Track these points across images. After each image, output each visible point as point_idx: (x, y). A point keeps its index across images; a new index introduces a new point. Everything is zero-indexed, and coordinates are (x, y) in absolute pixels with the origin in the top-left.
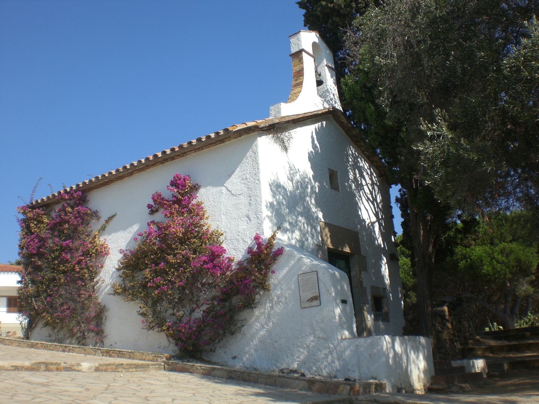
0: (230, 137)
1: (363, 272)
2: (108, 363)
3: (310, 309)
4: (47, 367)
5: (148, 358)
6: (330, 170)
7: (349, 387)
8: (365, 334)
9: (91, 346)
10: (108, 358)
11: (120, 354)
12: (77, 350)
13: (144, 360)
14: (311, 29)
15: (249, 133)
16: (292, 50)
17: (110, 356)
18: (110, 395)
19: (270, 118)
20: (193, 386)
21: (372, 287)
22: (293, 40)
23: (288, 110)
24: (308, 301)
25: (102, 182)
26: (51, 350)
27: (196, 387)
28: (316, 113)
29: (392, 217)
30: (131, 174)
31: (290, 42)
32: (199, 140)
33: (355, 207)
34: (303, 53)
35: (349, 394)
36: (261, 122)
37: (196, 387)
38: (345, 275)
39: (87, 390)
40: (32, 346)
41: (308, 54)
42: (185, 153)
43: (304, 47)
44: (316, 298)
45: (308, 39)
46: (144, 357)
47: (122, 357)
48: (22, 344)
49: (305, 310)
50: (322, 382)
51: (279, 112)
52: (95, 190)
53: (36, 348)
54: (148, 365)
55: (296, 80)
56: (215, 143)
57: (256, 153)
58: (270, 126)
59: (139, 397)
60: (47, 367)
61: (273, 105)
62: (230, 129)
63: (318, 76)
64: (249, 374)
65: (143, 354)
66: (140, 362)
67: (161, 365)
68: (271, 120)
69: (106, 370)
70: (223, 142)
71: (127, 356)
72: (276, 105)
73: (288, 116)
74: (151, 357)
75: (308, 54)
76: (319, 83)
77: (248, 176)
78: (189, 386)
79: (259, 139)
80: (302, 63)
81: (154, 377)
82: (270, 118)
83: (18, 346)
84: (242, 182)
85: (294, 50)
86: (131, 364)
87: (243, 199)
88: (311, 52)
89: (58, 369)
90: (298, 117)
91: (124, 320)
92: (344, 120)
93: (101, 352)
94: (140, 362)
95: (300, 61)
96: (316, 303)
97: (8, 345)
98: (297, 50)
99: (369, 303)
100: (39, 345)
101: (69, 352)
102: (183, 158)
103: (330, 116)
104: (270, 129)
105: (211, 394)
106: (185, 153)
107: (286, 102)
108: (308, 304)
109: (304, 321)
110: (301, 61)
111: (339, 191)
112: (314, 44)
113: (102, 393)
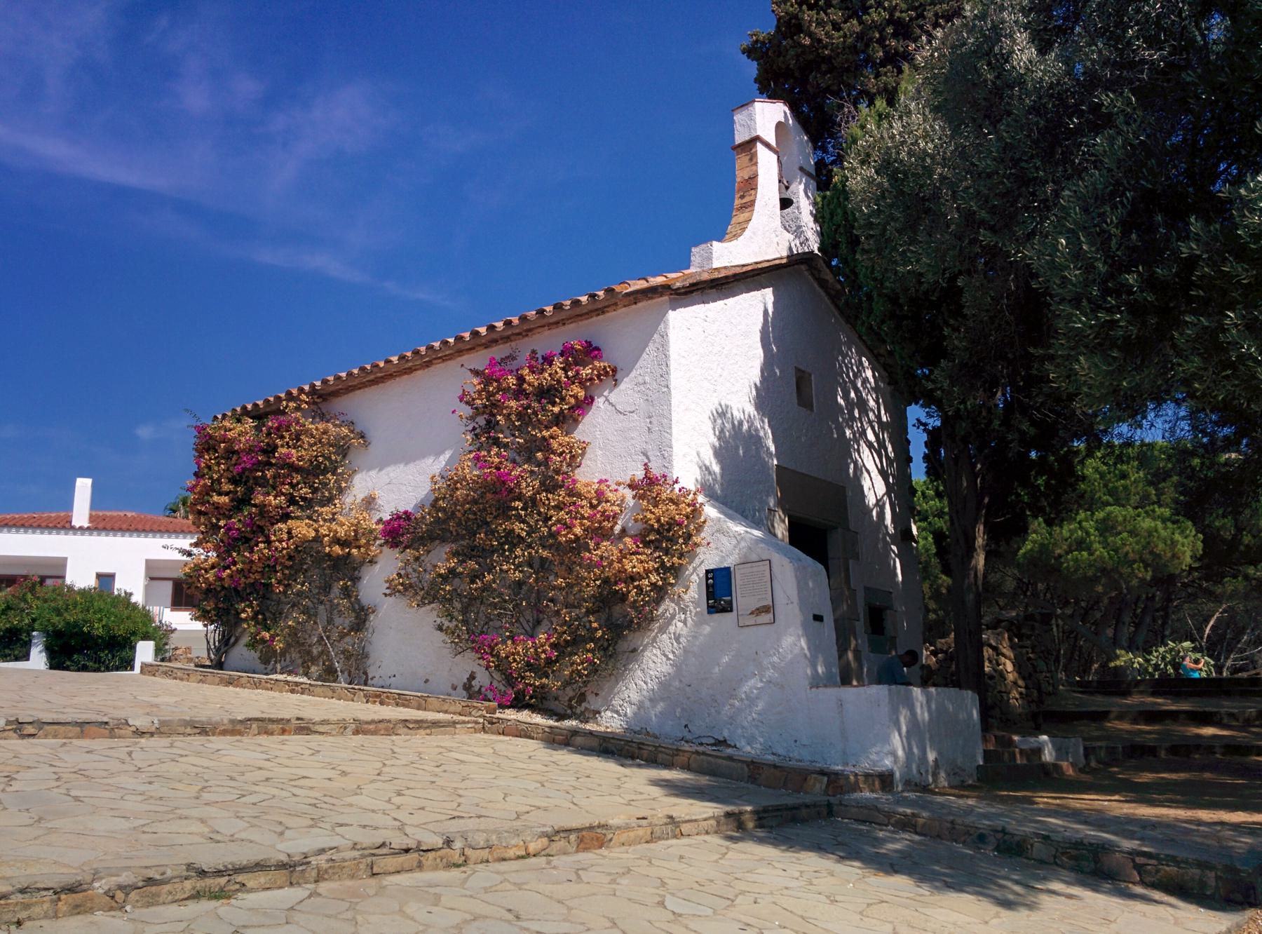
0: (616, 304)
1: (851, 562)
2: (376, 717)
3: (755, 628)
4: (267, 725)
5: (452, 709)
6: (798, 370)
7: (826, 779)
8: (855, 683)
9: (343, 685)
10: (377, 707)
11: (401, 701)
12: (318, 690)
13: (446, 712)
14: (773, 96)
15: (651, 298)
16: (737, 137)
17: (382, 703)
18: (386, 786)
19: (692, 270)
20: (539, 767)
21: (867, 589)
22: (739, 118)
23: (726, 255)
24: (752, 613)
25: (372, 377)
26: (267, 689)
27: (545, 769)
28: (777, 262)
29: (910, 460)
30: (428, 364)
31: (733, 122)
32: (558, 307)
33: (844, 451)
34: (759, 145)
35: (826, 793)
36: (675, 278)
37: (545, 769)
38: (821, 567)
39: (344, 774)
40: (230, 682)
41: (767, 145)
42: (530, 330)
43: (760, 132)
44: (765, 610)
45: (767, 116)
46: (446, 707)
47: (404, 706)
48: (210, 677)
49: (746, 630)
50: (775, 766)
51: (710, 259)
52: (358, 392)
53: (237, 686)
54: (455, 723)
55: (742, 197)
56: (587, 313)
57: (664, 336)
58: (692, 285)
59: (442, 788)
60: (267, 725)
61: (696, 246)
62: (618, 288)
63: (783, 189)
64: (640, 745)
65: (444, 700)
66: (441, 716)
67: (477, 723)
68: (691, 275)
69: (374, 733)
70: (603, 312)
71: (414, 703)
72: (703, 246)
73: (725, 268)
74: (459, 708)
75: (767, 145)
76: (785, 203)
77: (647, 379)
78: (532, 766)
79: (672, 315)
80: (756, 164)
81: (465, 748)
82: (692, 270)
83: (200, 681)
84: (636, 389)
85: (740, 137)
86: (422, 721)
87: (637, 421)
88: (773, 143)
89: (283, 732)
90: (745, 269)
91: (407, 636)
92: (829, 276)
93: (365, 696)
94: (441, 716)
95: (751, 159)
96: (766, 618)
97: (182, 679)
98: (747, 138)
99: (868, 638)
100: (244, 681)
101: (302, 693)
102: (526, 339)
103: (803, 267)
104: (692, 292)
105: (574, 783)
106: (530, 330)
107: (720, 240)
108: (751, 620)
109: (739, 644)
110: (753, 159)
111: (812, 410)
112: (780, 127)
113: (372, 782)
